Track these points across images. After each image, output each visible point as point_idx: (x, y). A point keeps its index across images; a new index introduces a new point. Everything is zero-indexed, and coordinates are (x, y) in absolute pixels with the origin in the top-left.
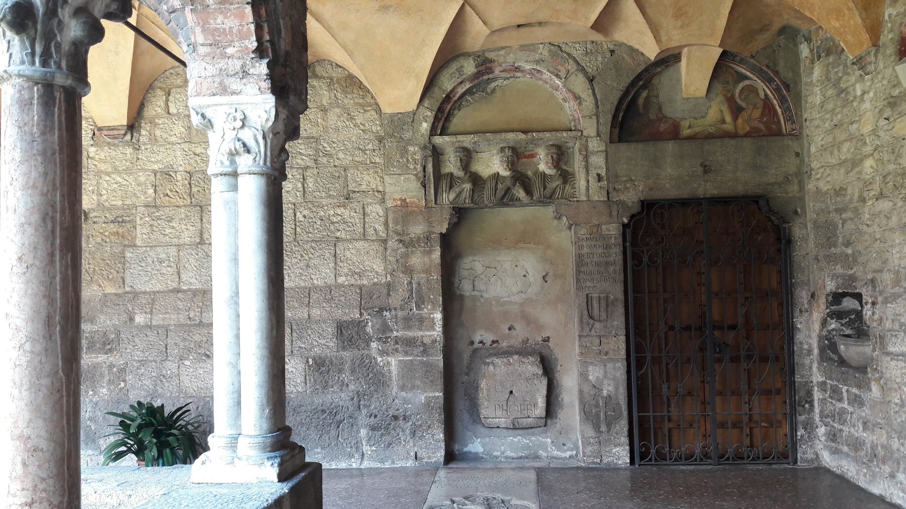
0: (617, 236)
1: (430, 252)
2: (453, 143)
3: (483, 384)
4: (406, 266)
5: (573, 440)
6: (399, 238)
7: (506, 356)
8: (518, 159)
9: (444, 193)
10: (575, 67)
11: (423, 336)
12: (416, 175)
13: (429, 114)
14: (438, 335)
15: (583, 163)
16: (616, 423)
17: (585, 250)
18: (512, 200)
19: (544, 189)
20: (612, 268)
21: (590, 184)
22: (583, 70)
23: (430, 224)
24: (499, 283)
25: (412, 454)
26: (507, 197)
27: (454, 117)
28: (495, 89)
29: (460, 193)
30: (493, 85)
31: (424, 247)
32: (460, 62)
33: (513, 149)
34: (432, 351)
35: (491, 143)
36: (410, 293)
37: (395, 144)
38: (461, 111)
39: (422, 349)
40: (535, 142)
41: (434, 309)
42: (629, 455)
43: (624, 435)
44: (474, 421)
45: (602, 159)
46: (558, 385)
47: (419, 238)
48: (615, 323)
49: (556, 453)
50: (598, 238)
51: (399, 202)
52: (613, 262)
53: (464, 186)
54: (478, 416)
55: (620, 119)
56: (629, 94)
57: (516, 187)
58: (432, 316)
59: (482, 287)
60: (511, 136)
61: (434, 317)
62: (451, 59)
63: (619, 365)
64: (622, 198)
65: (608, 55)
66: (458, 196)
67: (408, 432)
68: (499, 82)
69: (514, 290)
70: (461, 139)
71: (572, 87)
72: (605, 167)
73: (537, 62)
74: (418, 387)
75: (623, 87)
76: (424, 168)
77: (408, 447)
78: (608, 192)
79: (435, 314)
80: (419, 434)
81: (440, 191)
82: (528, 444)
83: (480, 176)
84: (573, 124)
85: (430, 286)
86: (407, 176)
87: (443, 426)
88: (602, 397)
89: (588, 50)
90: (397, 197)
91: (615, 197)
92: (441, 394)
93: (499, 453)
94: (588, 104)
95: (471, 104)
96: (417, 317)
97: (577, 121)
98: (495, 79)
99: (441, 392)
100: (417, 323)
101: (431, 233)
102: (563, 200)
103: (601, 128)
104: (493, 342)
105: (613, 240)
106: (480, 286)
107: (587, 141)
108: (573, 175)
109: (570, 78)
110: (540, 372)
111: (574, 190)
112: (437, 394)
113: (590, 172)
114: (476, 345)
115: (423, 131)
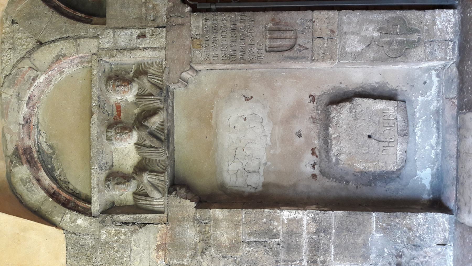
0: (204, 18)
1: (216, 221)
2: (99, 192)
3: (360, 166)
4: (230, 248)
5: (420, 73)
6: (199, 254)
7: (329, 141)
9: (152, 203)
10: (26, 61)
11: (308, 233)
12: (132, 233)
13: (68, 216)
14: (308, 216)
15: (126, 53)
16: (409, 24)
17: (219, 53)
20: (239, 24)
21: (148, 46)
22: (30, 53)
23: (184, 220)
24: (251, 145)
25: (440, 249)
26: (159, 135)
27: (76, 189)
28: (49, 145)
29: (153, 185)
30: (45, 147)
31: (210, 227)
32: (17, 182)
33: (110, 127)
34: (325, 224)
35: (101, 150)
36: (259, 245)
37: (98, 254)
38: (70, 181)
39: (322, 234)
40: (102, 104)
41: (278, 219)
42: (445, 10)
43: (422, 15)
44: (398, 177)
45: (122, 33)
46: (362, 87)
47: (200, 232)
48: (299, 21)
49: (434, 91)
50: (206, 39)
51: (161, 253)
52: (232, 23)
53: (146, 181)
54: (393, 172)
55: (83, 15)
57: (148, 125)
58: (286, 221)
59: (256, 163)
60: (94, 130)
61: (287, 219)
62: (13, 191)
63: (345, 19)
64: (163, 12)
65: (17, 26)
66: (155, 187)
67: (414, 253)
68: (42, 140)
69: (259, 130)
71: (46, 64)
72: (130, 30)
73: (20, 100)
74: (364, 240)
75: (49, 11)
77: (432, 253)
78: (157, 27)
79: (284, 218)
80: (417, 241)
81: (150, 207)
82: (423, 121)
83: (138, 163)
84: (86, 65)
85: (253, 222)
86: (133, 243)
87: (409, 213)
88: (381, 37)
89: (11, 47)
90: (154, 254)
91: (163, 20)
92: (374, 214)
93: (433, 151)
94: (64, 48)
95: (63, 170)
96: (287, 238)
97: (83, 60)
98: (39, 145)
99: (371, 214)
100: (294, 238)
101: (195, 219)
102: (164, 75)
103: (90, 34)
104: (313, 153)
105: (209, 23)
106: (253, 165)
108: (139, 64)
109: (38, 66)
110: (347, 105)
111: (154, 63)
112: (374, 219)
113: (135, 46)
114: (317, 172)
115: (86, 223)
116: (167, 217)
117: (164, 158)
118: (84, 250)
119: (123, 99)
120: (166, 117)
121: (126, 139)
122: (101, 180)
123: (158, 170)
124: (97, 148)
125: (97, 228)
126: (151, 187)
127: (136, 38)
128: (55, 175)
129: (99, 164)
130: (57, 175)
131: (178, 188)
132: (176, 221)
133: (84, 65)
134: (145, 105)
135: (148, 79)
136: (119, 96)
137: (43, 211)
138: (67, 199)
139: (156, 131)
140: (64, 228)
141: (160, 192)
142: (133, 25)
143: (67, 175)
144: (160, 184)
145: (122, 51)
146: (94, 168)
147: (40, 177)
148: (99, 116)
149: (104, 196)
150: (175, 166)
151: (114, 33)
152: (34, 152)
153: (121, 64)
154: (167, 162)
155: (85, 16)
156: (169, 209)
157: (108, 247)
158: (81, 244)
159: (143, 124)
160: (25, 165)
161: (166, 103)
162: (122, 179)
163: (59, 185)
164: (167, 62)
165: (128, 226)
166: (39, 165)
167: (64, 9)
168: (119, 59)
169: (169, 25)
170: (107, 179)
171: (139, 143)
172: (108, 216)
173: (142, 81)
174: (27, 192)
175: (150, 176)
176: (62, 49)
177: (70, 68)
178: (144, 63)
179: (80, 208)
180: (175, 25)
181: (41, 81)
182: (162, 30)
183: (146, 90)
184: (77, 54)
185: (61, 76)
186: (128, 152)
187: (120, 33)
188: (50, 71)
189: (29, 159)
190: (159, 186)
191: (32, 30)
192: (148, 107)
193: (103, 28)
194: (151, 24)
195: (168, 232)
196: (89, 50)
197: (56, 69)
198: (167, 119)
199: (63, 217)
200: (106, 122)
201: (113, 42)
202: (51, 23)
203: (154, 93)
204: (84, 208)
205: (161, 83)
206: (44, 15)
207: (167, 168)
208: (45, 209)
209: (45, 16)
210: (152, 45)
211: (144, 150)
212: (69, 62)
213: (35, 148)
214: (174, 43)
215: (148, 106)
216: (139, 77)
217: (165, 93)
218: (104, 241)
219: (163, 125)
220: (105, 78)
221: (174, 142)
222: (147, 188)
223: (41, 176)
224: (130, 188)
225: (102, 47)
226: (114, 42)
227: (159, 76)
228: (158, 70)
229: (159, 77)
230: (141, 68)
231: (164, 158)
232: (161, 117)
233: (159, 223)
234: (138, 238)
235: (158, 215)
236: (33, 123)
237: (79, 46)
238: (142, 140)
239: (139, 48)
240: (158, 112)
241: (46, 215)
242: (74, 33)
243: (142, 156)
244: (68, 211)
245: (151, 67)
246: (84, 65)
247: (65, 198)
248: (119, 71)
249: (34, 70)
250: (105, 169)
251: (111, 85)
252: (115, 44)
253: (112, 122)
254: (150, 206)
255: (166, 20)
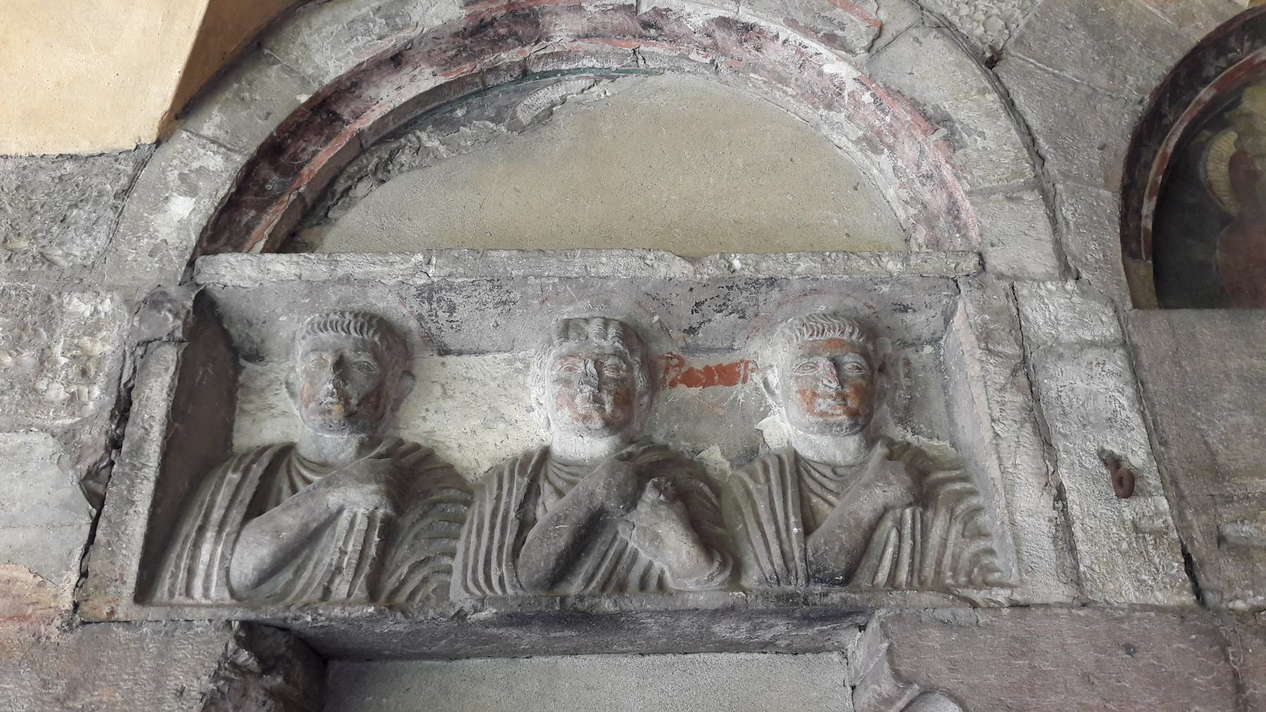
2: (314, 288)
8: (654, 385)
9: (210, 535)
12: (67, 437)
15: (1016, 399)
18: (615, 583)
19: (808, 528)
21: (1075, 510)
26: (588, 565)
27: (347, 208)
28: (550, 113)
29: (309, 538)
30: (545, 96)
33: (632, 335)
35: (516, 295)
40: (740, 299)
45: (1111, 382)
53: (334, 499)
55: (1148, 223)
56: (1165, 130)
57: (643, 508)
68: (575, 85)
70: (358, 272)
71: (906, 80)
72: (1136, 420)
76: (123, 409)
83: (449, 467)
94: (991, 145)
97: (942, 223)
102: (927, 598)
103: (1073, 243)
107: (1013, 294)
108: (962, 469)
111: (983, 544)
113: (1060, 444)
116: (111, 619)
117: (459, 597)
118: (38, 226)
119: (772, 393)
120: (690, 605)
121: (571, 403)
122: (372, 293)
123: (390, 565)
124: (525, 277)
125: (134, 278)
126: (296, 529)
127: (1103, 451)
128: (418, 133)
129: (451, 288)
130: (418, 138)
131: (279, 680)
132: (76, 671)
133: (919, 227)
134: (749, 494)
135: (893, 508)
136: (783, 375)
137: (260, 71)
138: (301, 167)
139: (611, 552)
140: (164, 146)
141: (267, 574)
142: (1171, 432)
143: (417, 174)
144: (312, 578)
145: (1022, 379)
146: (429, 263)
147: (409, 69)
148: (679, 284)
149: (291, 311)
150: (428, 663)
151: (1105, 345)
152: (521, 52)
153: (945, 388)
154: (431, 613)
155: (1146, 230)
156: (154, 632)
157: (26, 325)
158: (75, 212)
159: (650, 484)
160: (464, 12)
161: (772, 606)
162: (368, 386)
163: (373, 145)
164: (1006, 611)
165: (106, 415)
166: (467, 68)
167: (1156, 152)
168: (974, 369)
169: (1217, 622)
170: (374, 322)
171: (551, 470)
172: (179, 323)
173: (881, 477)
174: (350, 19)
175: (361, 524)
176: (982, 134)
177: (896, 175)
178: (973, 493)
179: (253, 213)
180: (1227, 659)
181: (828, 69)
182: (1182, 586)
183: (830, 497)
184: (969, 194)
185: (857, 142)
186: (505, 421)
187: (1111, 373)
188: (873, 95)
189: (491, 32)
190: (298, 573)
191: (1044, 32)
192: (739, 509)
193: (1116, 298)
194: (1195, 523)
195: (25, 625)
196: (995, 241)
197: (888, 119)
198: (676, 613)
199: (213, 142)
200: (656, 318)
201: (1056, 339)
202: (1089, 97)
203: (817, 537)
204: (249, 228)
205: (882, 576)
206: (1118, 73)
207: (399, 614)
208: (266, 79)
209: (1112, 76)
210: (1084, 531)
211: (510, 490)
212: (925, 168)
213: (539, 58)
214: (1121, 653)
215: (747, 510)
216: (901, 465)
217: (825, 600)
218: (61, 306)
219: (643, 585)
220: (868, 312)
221: (555, 654)
222: (298, 505)
223: (416, 72)
224: (317, 425)
225: (1025, 292)
226: (1060, 344)
227: (920, 571)
228: (947, 560)
229: (912, 565)
230: (941, 475)
231: (459, 597)
232: (690, 577)
233: (84, 574)
234: (31, 468)
235: (134, 566)
236: (642, 48)
237: (1010, 199)
238: (564, 480)
239: (1055, 463)
240: (718, 559)
241: (239, 82)
242: (1065, 181)
243: (482, 487)
244: (240, 160)
245: (957, 528)
246: (919, 227)
247: (306, 157)
248: (907, 375)
249: (874, 40)
250: (425, 314)
251: (837, 335)
252: (1050, 350)
253: (654, 347)
254: (199, 523)
255: (1240, 605)
